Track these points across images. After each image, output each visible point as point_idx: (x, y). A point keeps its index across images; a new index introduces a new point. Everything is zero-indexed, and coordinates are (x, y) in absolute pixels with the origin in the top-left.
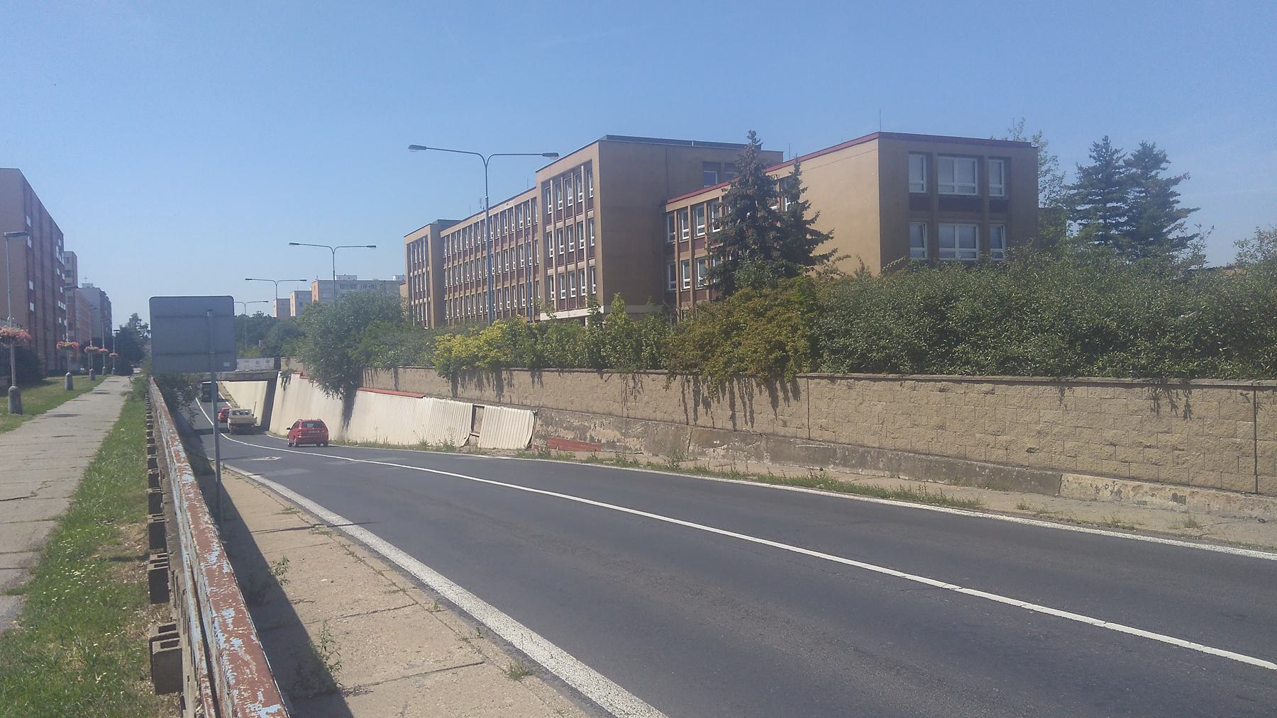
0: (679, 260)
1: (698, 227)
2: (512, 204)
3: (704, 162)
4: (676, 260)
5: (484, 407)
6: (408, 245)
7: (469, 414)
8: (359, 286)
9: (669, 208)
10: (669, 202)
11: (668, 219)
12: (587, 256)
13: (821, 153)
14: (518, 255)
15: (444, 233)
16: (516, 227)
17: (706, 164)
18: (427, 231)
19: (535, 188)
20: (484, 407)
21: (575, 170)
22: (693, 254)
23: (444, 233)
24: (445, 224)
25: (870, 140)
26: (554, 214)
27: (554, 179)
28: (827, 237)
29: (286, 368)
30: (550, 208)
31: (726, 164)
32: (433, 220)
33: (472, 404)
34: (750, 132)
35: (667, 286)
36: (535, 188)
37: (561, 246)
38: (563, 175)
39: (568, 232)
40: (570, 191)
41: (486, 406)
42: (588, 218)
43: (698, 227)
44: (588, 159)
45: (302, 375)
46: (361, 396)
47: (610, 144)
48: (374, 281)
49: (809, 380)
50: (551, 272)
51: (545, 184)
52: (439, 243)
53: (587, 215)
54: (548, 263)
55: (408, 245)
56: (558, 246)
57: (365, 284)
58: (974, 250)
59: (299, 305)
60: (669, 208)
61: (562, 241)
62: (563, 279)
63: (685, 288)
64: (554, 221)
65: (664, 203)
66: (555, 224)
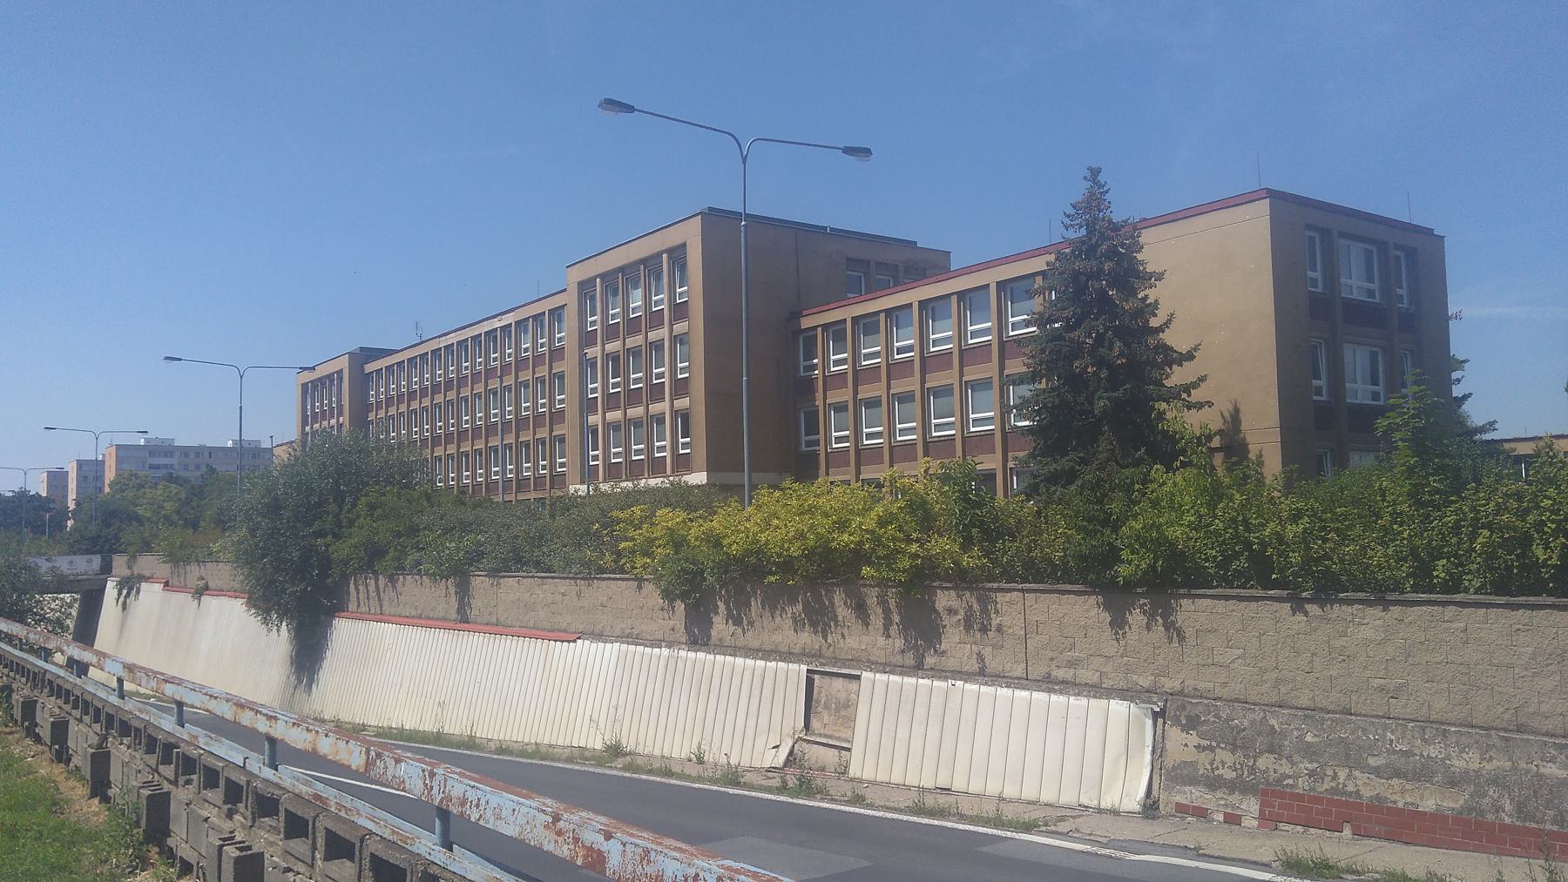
0: (825, 402)
1: (863, 351)
2: (509, 319)
3: (848, 259)
4: (819, 402)
5: (858, 678)
6: (304, 386)
7: (791, 696)
8: (177, 453)
9: (806, 323)
10: (805, 313)
11: (801, 340)
12: (671, 394)
13: (1018, 258)
14: (474, 406)
15: (369, 368)
16: (408, 386)
17: (852, 262)
18: (343, 363)
19: (565, 290)
20: (858, 678)
21: (330, 377)
22: (856, 393)
23: (370, 367)
24: (365, 355)
25: (1196, 215)
26: (602, 331)
27: (603, 276)
28: (1190, 356)
29: (127, 572)
30: (427, 379)
31: (876, 263)
32: (354, 347)
33: (804, 668)
34: (1090, 169)
35: (800, 444)
36: (565, 290)
37: (414, 429)
38: (622, 269)
39: (628, 359)
40: (639, 293)
41: (865, 675)
42: (626, 348)
43: (863, 351)
44: (679, 242)
45: (166, 584)
46: (344, 631)
47: (715, 220)
48: (200, 446)
49: (1026, 595)
50: (594, 419)
51: (585, 287)
52: (362, 381)
53: (603, 350)
54: (589, 406)
55: (304, 386)
56: (608, 380)
57: (186, 451)
58: (1375, 388)
59: (82, 479)
60: (806, 323)
61: (427, 420)
62: (453, 460)
63: (834, 446)
64: (603, 340)
65: (796, 316)
66: (603, 345)
